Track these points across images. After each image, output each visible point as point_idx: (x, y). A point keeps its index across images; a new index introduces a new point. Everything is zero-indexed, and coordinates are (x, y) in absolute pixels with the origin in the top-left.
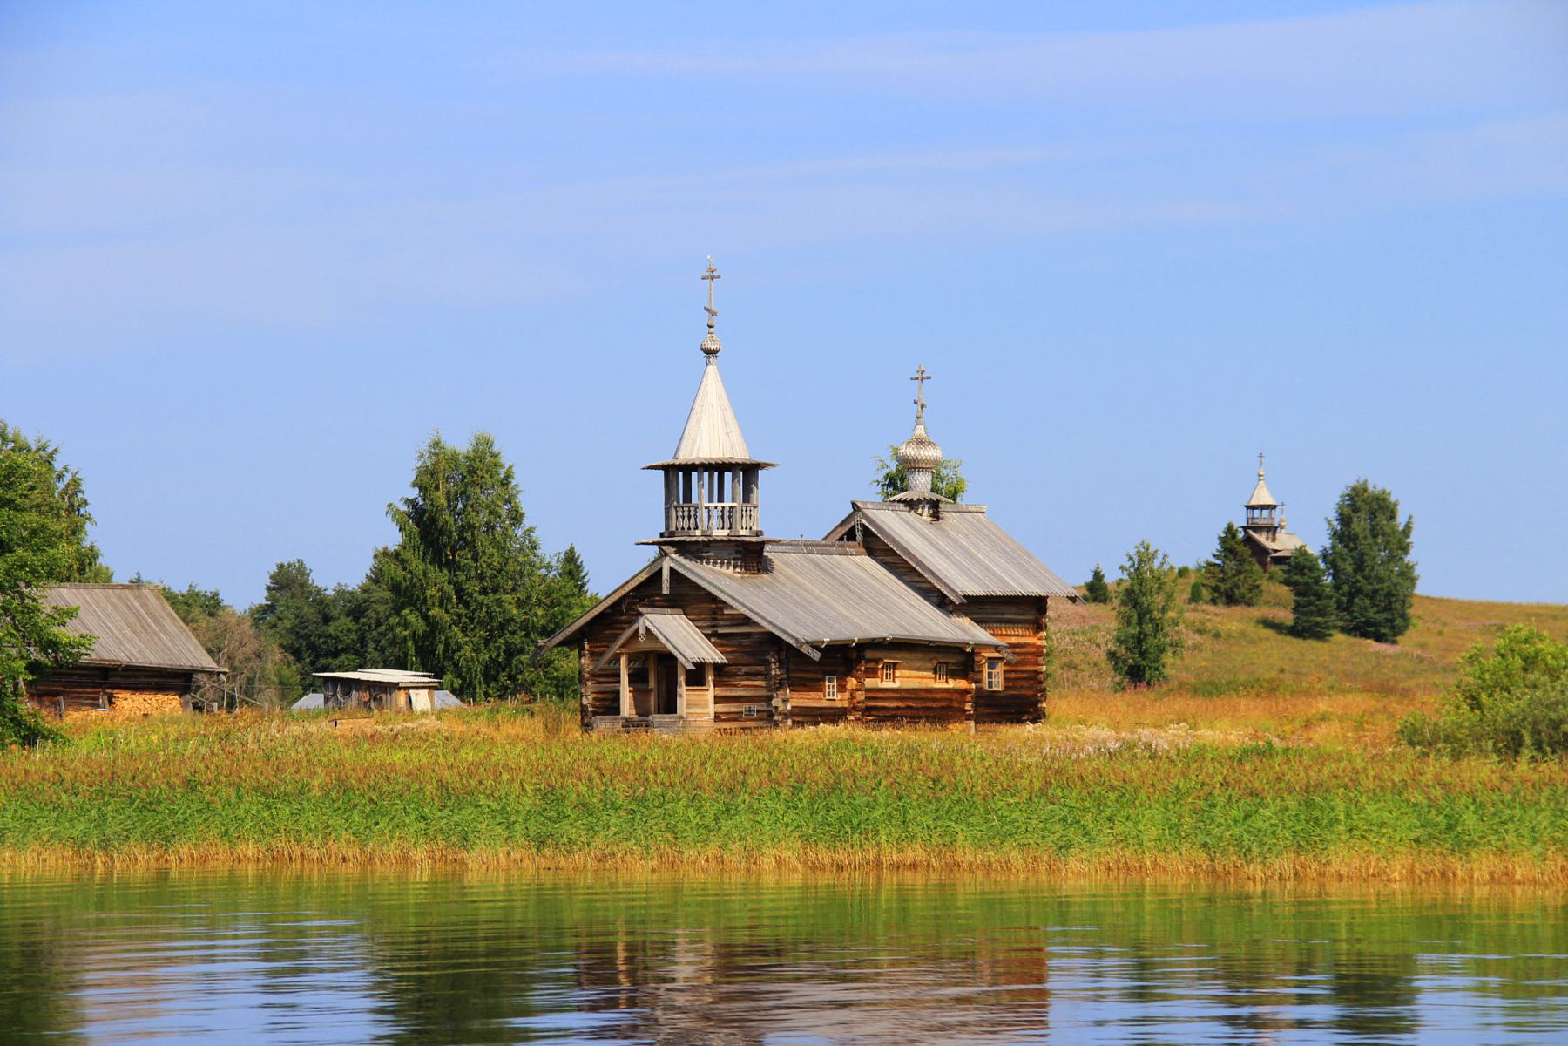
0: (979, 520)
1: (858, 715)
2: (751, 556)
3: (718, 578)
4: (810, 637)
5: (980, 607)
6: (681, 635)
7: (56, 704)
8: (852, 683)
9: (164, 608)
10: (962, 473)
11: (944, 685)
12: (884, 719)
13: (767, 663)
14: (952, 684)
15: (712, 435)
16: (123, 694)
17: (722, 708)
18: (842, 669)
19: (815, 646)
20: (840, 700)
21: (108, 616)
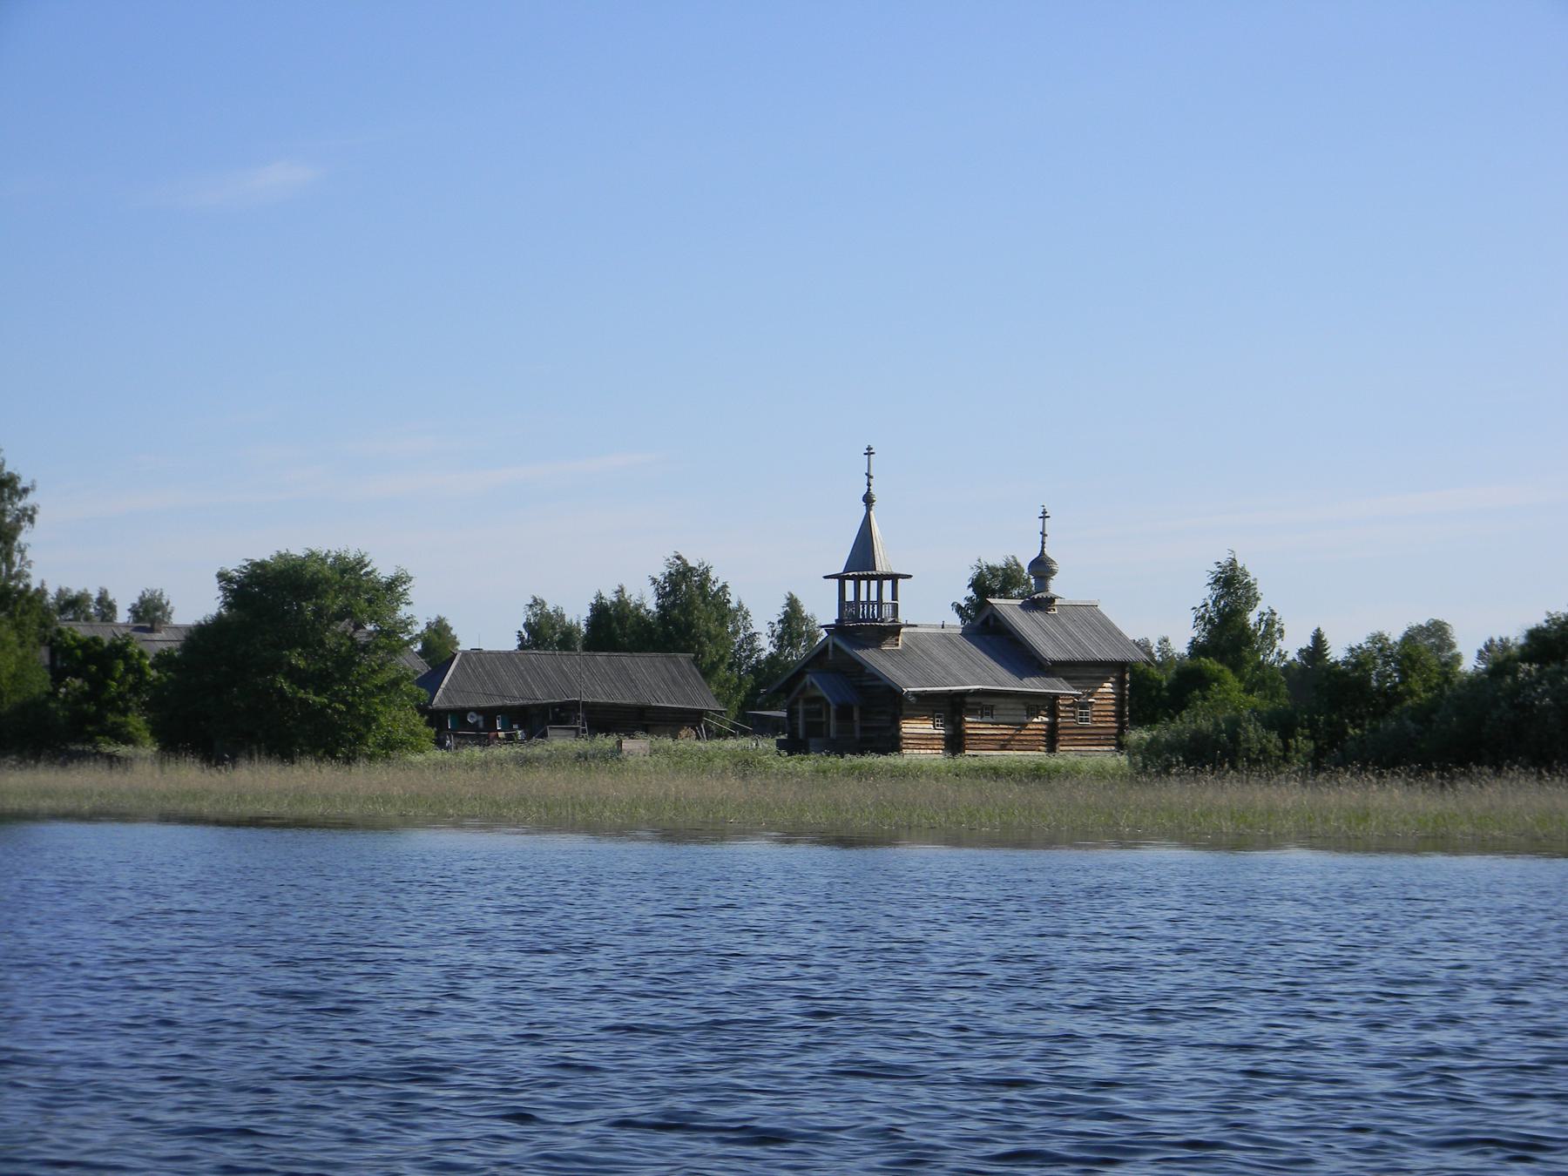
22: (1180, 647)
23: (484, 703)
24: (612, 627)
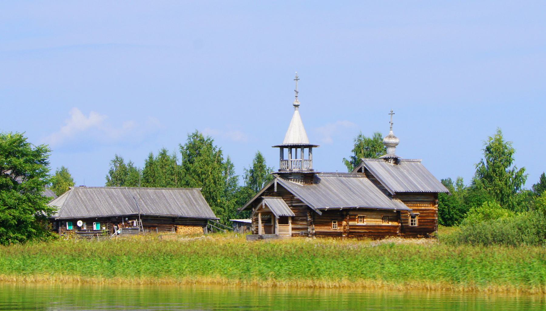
0: (417, 165)
1: (346, 234)
2: (310, 178)
3: (295, 187)
4: (321, 206)
5: (404, 196)
6: (278, 206)
7: (155, 230)
8: (344, 223)
9: (200, 197)
10: (513, 146)
11: (388, 224)
12: (361, 236)
13: (306, 216)
14: (390, 224)
15: (296, 135)
16: (180, 227)
17: (294, 232)
18: (341, 218)
19: (322, 210)
20: (339, 229)
21: (178, 199)
22: (467, 183)
23: (86, 215)
24: (157, 173)
